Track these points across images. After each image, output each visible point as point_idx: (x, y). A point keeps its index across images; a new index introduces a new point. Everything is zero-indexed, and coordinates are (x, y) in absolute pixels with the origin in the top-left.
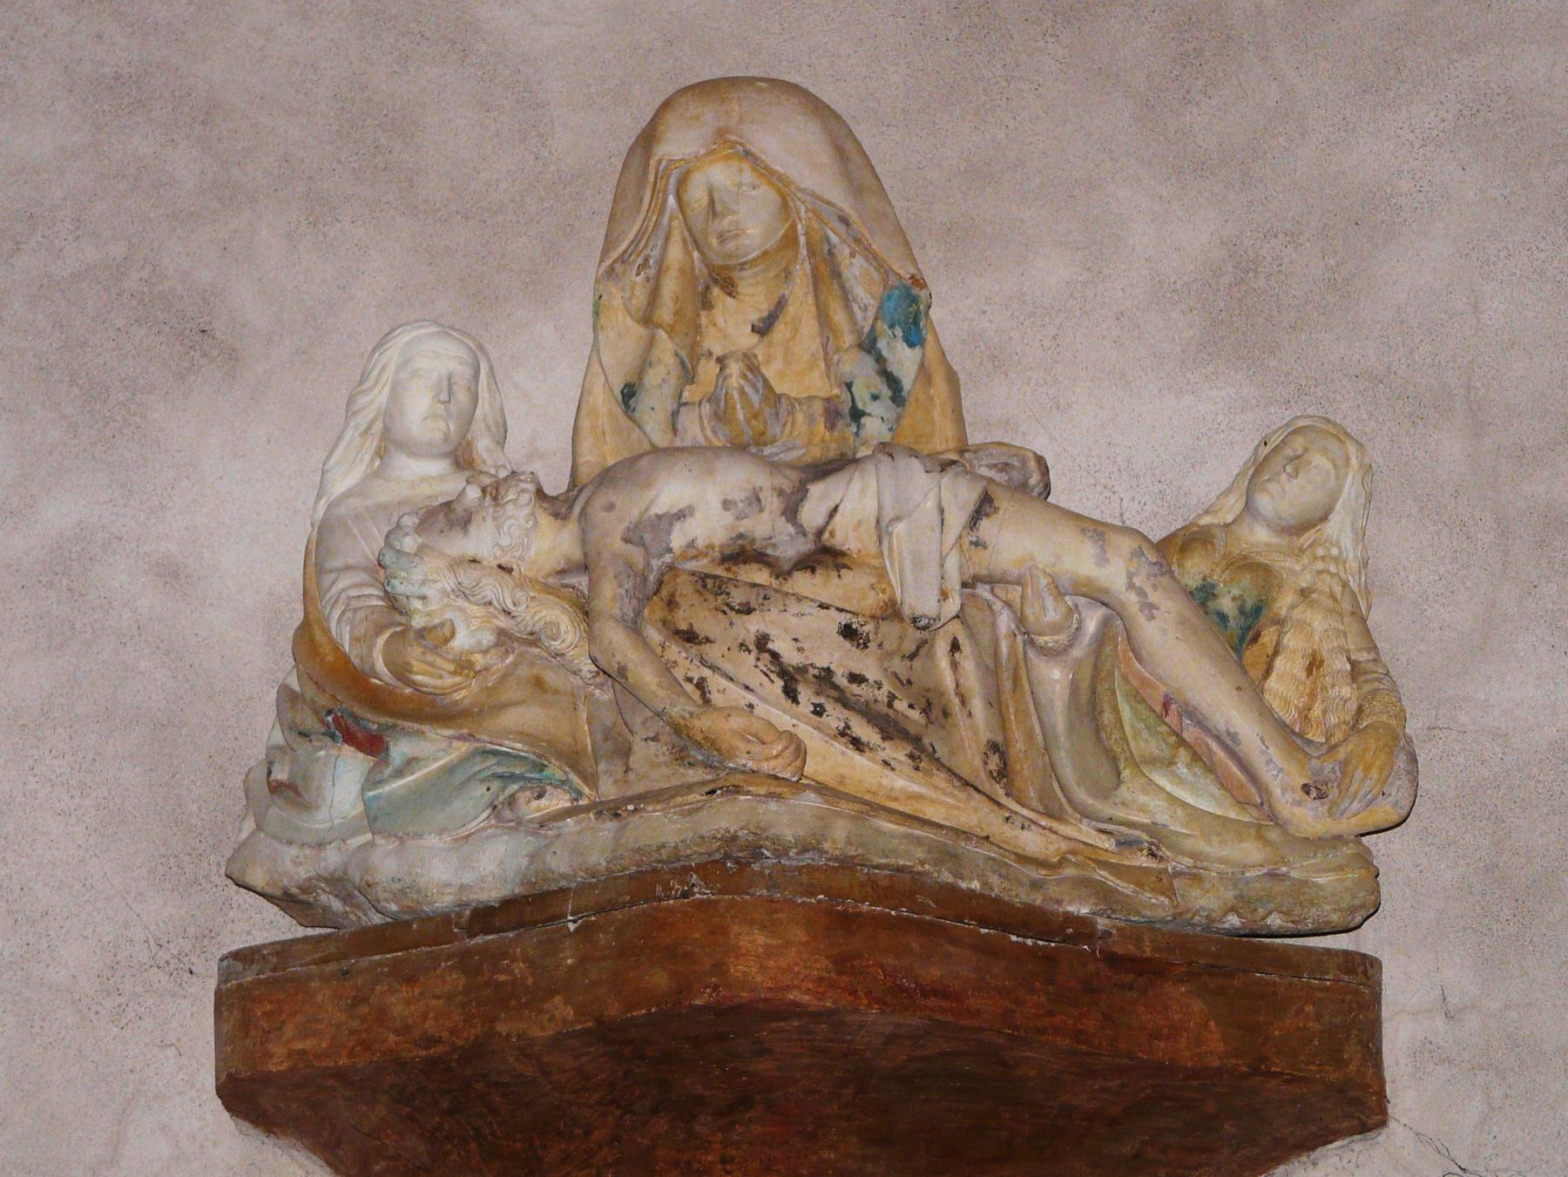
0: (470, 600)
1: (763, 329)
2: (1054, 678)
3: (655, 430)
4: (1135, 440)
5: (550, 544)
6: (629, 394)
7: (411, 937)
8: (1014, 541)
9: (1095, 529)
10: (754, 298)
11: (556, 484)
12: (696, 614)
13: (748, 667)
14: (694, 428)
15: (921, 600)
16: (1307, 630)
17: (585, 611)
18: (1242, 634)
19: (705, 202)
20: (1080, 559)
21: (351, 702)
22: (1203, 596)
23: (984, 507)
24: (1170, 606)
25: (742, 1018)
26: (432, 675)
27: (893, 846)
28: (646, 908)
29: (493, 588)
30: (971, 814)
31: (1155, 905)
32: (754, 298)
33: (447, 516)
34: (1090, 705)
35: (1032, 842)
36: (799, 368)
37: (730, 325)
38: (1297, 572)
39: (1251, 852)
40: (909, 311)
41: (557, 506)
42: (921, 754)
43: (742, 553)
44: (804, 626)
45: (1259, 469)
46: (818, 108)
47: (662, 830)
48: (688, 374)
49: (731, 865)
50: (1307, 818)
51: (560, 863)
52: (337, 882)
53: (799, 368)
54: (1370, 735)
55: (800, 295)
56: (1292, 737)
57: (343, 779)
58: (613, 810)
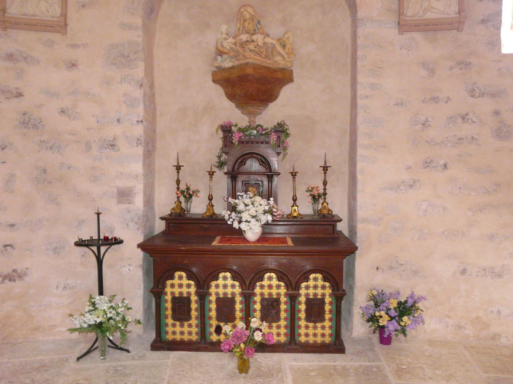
0: (228, 44)
1: (249, 24)
2: (270, 50)
3: (241, 31)
4: (275, 30)
5: (233, 41)
6: (239, 29)
7: (224, 70)
8: (267, 40)
9: (273, 39)
10: (248, 22)
11: (234, 36)
12: (244, 46)
13: (247, 50)
14: (244, 31)
15: (260, 44)
16: (288, 46)
17: (236, 45)
18: (284, 46)
19: (77, 333)
20: (272, 41)
21: (220, 53)
22: (281, 43)
23: (265, 37)
24: (278, 44)
25: (247, 75)
26: (225, 51)
27: (258, 62)
28: (241, 67)
29: (229, 44)
30: (264, 60)
31: (277, 66)
32: (248, 22)
33: (226, 39)
34: (272, 52)
35: (268, 62)
36: (251, 27)
37: (246, 24)
38: (287, 42)
39: (284, 62)
40: (259, 22)
41: (234, 38)
42: (260, 56)
43: (247, 41)
44: (251, 46)
45: (284, 34)
46: (252, 7)
47: (242, 62)
48: (243, 28)
49: (247, 64)
50: (288, 60)
51: (235, 64)
52: (219, 66)
53: (251, 27)
54: (292, 53)
55: (251, 21)
56: (287, 54)
57: (219, 58)
58: (238, 60)
